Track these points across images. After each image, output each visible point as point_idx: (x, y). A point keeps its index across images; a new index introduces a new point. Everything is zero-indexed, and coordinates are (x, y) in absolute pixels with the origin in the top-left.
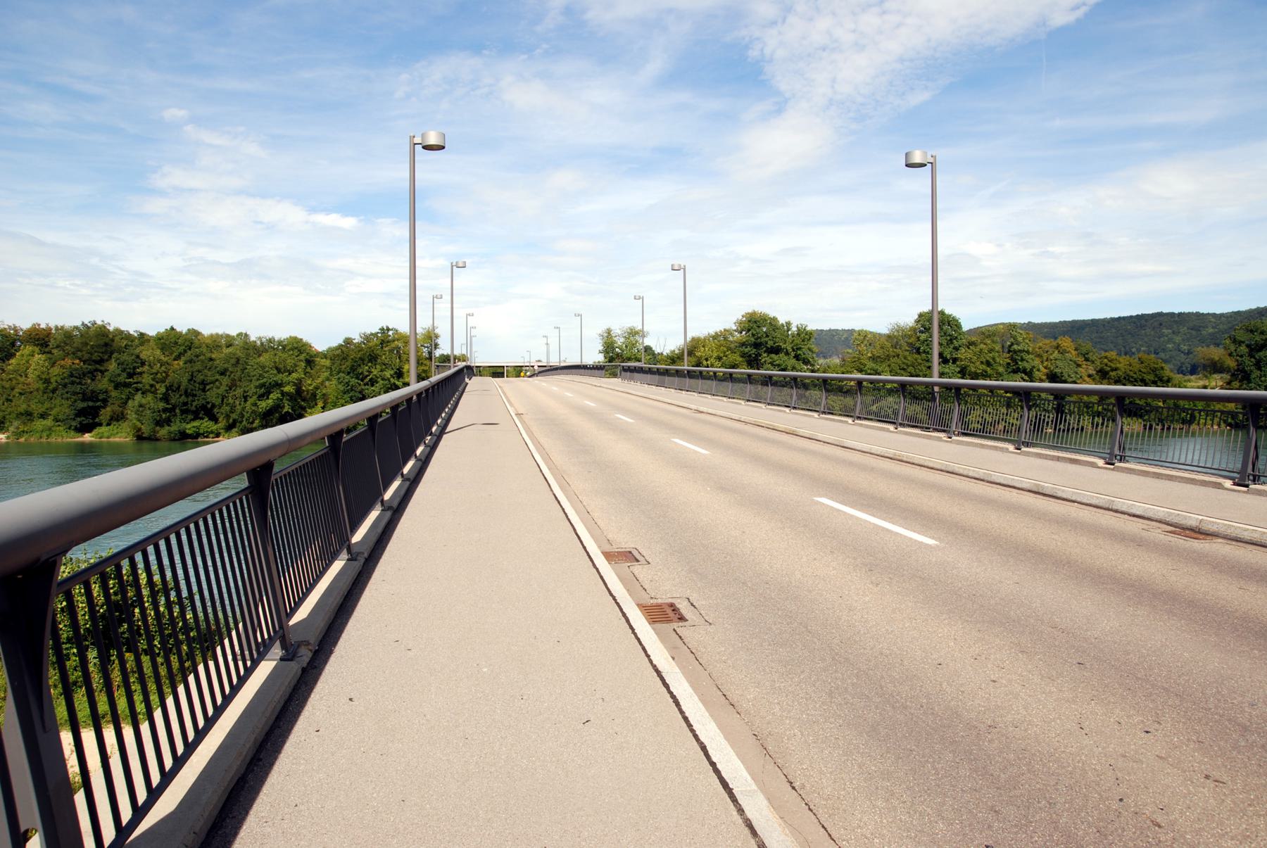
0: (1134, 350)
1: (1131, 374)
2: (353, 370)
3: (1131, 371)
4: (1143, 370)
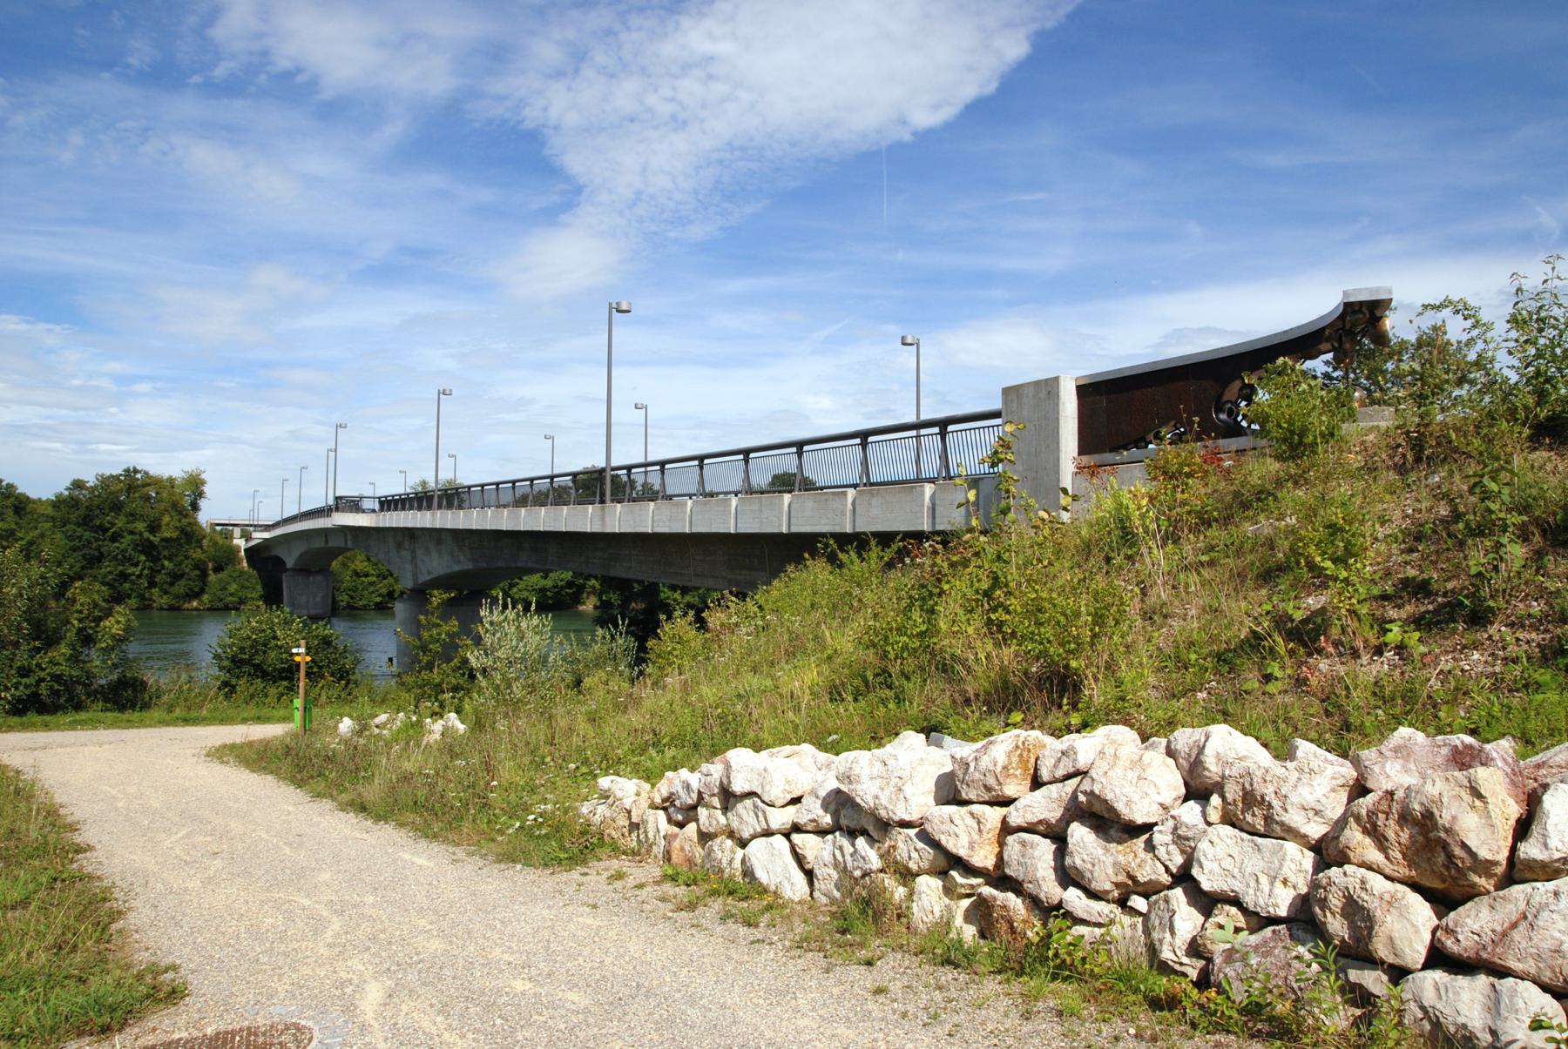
2: (86, 521)
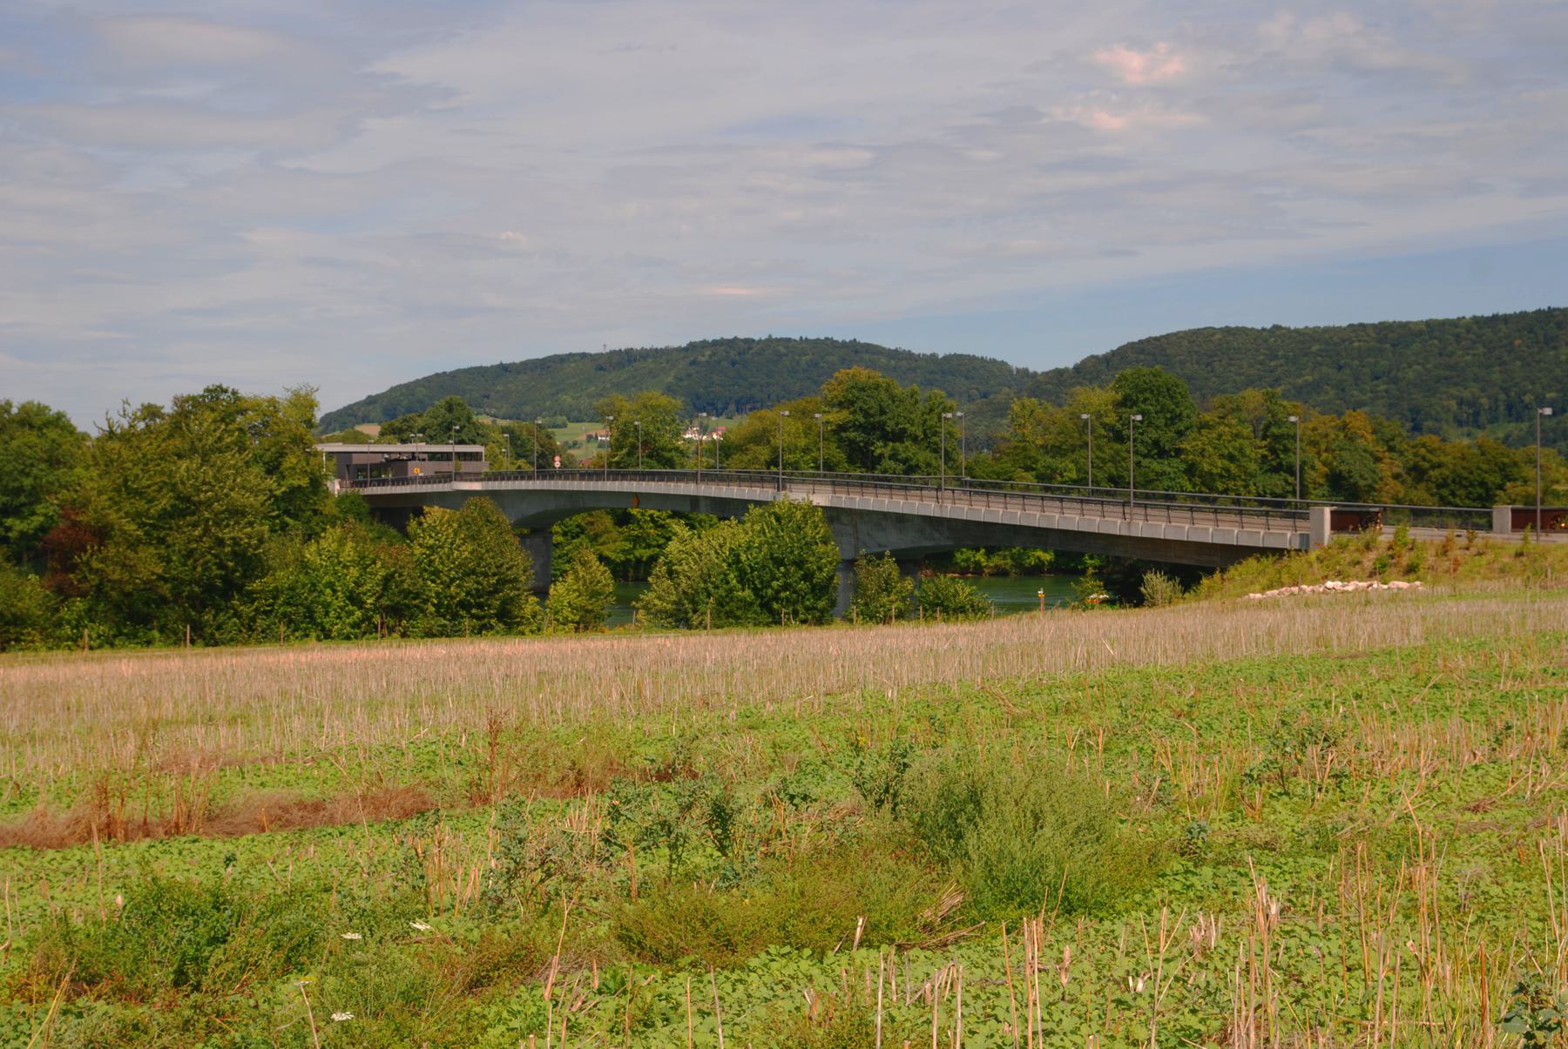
0: (1528, 398)
1: (1465, 474)
3: (1464, 468)
4: (1485, 467)
